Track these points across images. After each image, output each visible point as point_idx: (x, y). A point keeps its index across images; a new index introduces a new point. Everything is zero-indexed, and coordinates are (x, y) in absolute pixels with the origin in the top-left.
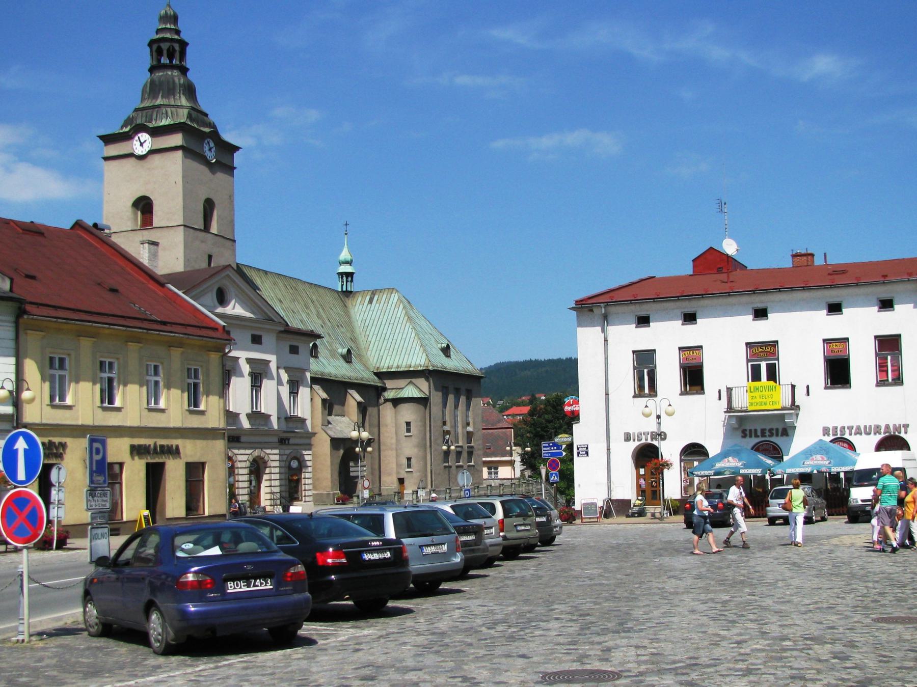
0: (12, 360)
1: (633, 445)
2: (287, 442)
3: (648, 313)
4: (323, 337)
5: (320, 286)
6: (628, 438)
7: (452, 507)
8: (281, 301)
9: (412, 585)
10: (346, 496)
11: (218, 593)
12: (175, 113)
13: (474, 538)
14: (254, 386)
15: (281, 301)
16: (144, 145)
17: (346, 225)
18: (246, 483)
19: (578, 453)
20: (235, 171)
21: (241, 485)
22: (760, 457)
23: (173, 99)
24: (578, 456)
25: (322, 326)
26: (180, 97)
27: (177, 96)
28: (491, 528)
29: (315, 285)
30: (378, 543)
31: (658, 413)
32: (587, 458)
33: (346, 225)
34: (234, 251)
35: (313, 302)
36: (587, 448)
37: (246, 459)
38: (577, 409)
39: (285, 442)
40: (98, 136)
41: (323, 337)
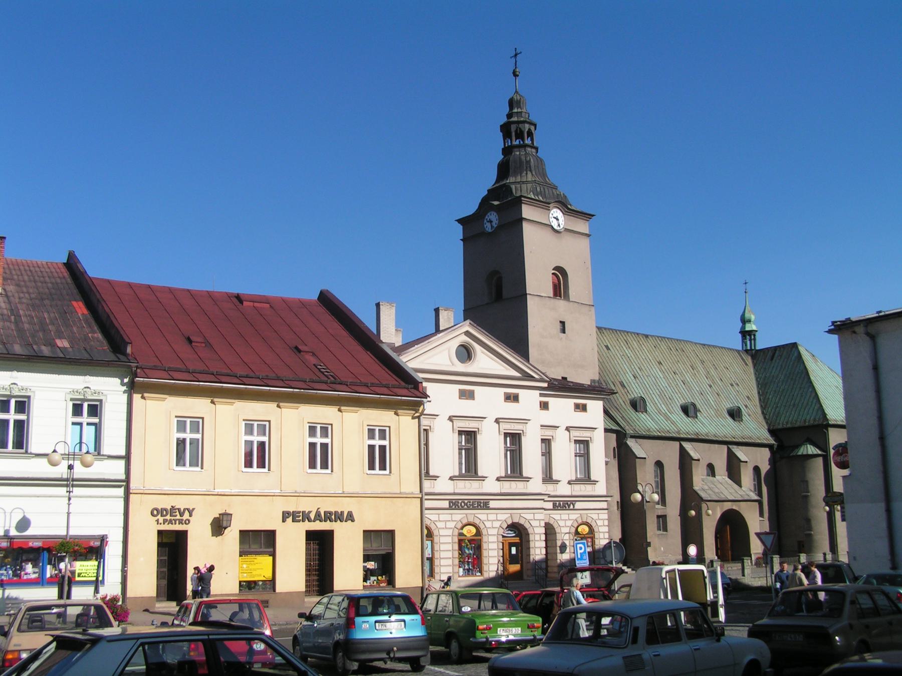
0: (830, 429)
2: (572, 507)
5: (713, 346)
8: (660, 363)
9: (225, 672)
10: (366, 569)
12: (519, 189)
15: (660, 363)
17: (746, 283)
20: (462, 238)
21: (443, 555)
23: (519, 177)
25: (710, 386)
26: (527, 174)
27: (524, 174)
28: (7, 615)
29: (709, 346)
33: (746, 283)
35: (702, 362)
39: (569, 506)
40: (456, 220)
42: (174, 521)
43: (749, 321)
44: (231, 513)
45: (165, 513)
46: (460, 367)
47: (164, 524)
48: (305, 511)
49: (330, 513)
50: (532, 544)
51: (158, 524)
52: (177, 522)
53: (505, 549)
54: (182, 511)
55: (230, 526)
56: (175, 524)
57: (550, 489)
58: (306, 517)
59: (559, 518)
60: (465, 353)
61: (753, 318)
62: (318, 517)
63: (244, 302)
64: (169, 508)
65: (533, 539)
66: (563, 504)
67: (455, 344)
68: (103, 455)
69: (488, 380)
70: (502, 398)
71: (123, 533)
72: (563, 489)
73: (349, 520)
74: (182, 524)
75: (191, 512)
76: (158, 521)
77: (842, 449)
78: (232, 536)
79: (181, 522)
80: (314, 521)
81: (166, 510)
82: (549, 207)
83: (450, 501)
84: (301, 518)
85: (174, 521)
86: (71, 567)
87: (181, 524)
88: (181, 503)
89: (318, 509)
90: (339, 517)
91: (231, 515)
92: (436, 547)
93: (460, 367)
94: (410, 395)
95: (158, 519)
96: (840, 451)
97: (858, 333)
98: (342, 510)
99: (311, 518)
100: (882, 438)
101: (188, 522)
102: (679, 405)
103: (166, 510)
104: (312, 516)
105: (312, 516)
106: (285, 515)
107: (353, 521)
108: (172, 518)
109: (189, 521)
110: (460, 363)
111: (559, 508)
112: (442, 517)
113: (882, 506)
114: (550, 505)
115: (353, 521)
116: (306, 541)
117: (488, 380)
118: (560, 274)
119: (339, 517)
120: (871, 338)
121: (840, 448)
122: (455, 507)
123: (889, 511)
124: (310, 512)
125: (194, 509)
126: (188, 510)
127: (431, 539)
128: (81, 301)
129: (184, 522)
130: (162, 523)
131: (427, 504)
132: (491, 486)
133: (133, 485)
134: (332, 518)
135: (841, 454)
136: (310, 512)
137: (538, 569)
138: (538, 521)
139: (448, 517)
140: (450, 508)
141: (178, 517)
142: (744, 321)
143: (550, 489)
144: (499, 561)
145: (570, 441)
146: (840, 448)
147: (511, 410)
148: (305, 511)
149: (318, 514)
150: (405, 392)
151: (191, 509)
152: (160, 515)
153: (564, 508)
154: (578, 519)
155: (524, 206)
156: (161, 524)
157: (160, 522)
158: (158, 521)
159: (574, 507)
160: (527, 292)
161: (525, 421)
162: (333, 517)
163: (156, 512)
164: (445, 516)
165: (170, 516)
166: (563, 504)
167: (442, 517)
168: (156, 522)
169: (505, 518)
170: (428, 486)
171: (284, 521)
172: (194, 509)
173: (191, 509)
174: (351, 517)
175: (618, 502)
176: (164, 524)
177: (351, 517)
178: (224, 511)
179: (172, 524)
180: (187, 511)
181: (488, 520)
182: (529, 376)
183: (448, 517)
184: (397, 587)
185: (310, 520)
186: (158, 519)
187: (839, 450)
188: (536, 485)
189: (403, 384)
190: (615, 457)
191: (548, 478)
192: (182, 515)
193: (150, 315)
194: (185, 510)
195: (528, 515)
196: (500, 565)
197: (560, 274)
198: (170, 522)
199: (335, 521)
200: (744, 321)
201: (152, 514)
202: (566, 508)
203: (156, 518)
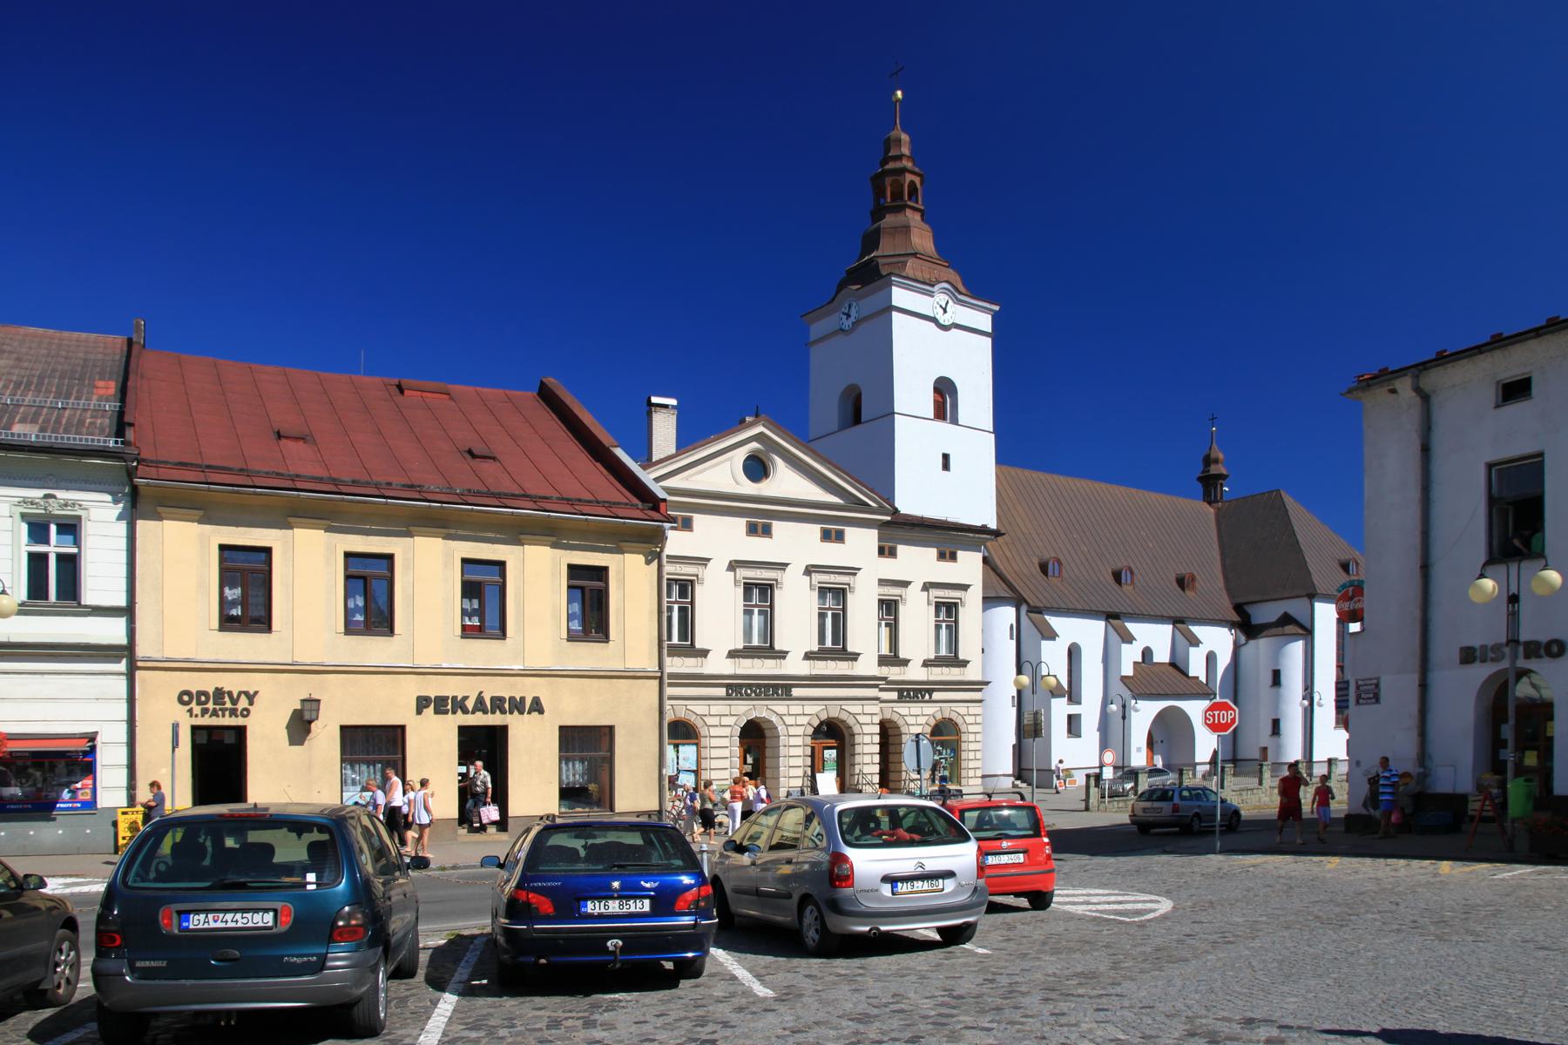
1: (1480, 673)
2: (927, 697)
3: (1527, 370)
4: (1004, 534)
6: (1468, 656)
7: (585, 847)
11: (288, 963)
13: (164, 965)
14: (883, 619)
16: (948, 309)
18: (894, 751)
19: (1358, 698)
22: (151, 841)
24: (1358, 703)
30: (1156, 830)
31: (1514, 590)
32: (1376, 706)
34: (850, 427)
36: (1377, 686)
37: (805, 723)
38: (1358, 606)
39: (923, 697)
41: (1004, 534)
42: (220, 713)
43: (1216, 461)
44: (317, 698)
45: (203, 698)
46: (749, 488)
47: (203, 716)
48: (456, 697)
49: (501, 699)
50: (858, 749)
51: (191, 716)
52: (227, 713)
53: (821, 760)
54: (235, 696)
55: (317, 719)
56: (223, 716)
57: (894, 673)
58: (459, 705)
59: (907, 713)
60: (757, 468)
61: (1221, 456)
62: (480, 705)
63: (406, 392)
64: (211, 691)
65: (861, 742)
66: (913, 693)
67: (741, 455)
68: (86, 606)
69: (795, 511)
70: (818, 535)
71: (128, 733)
72: (915, 673)
73: (535, 711)
74: (237, 716)
75: (251, 698)
76: (190, 711)
77: (1353, 590)
78: (326, 737)
79: (233, 712)
80: (473, 713)
81: (205, 694)
82: (933, 292)
83: (728, 686)
84: (449, 707)
85: (220, 713)
86: (843, 787)
87: (233, 716)
88: (232, 683)
89: (481, 692)
90: (517, 706)
91: (319, 701)
92: (704, 753)
93: (749, 488)
94: (641, 517)
95: (192, 709)
96: (1350, 594)
97: (1337, 561)
98: (523, 695)
99: (466, 708)
100: (1425, 568)
101: (246, 713)
102: (1110, 571)
103: (185, 694)
104: (470, 704)
105: (470, 704)
106: (422, 703)
107: (541, 711)
108: (218, 707)
109: (248, 710)
110: (750, 482)
111: (908, 699)
112: (714, 710)
113: (1414, 678)
114: (894, 695)
115: (541, 711)
116: (560, 750)
117: (795, 511)
118: (945, 392)
119: (517, 706)
120: (1422, 398)
121: (1351, 589)
122: (736, 695)
123: (1424, 686)
124: (465, 698)
125: (256, 693)
126: (246, 693)
127: (696, 741)
128: (116, 382)
129: (239, 713)
130: (200, 715)
131: (669, 691)
132: (795, 665)
133: (142, 650)
134: (505, 708)
135: (1351, 599)
136: (465, 698)
137: (865, 784)
138: (870, 716)
139: (725, 710)
140: (728, 697)
141: (229, 705)
142: (1208, 461)
143: (894, 673)
144: (805, 772)
145: (928, 604)
146: (1351, 589)
147: (831, 554)
148: (456, 697)
149: (480, 701)
150: (638, 514)
151: (252, 693)
152: (194, 701)
153: (916, 699)
154: (935, 715)
155: (894, 289)
156: (196, 716)
157: (195, 712)
158: (190, 711)
159: (930, 697)
160: (896, 411)
161: (852, 571)
162: (507, 706)
163: (185, 698)
164: (718, 708)
165: (214, 704)
166: (913, 693)
167: (714, 710)
168: (188, 714)
169: (816, 712)
170: (675, 665)
171: (419, 712)
172: (256, 693)
173: (252, 693)
174: (537, 707)
175: (1013, 697)
176: (203, 716)
177: (537, 707)
178: (308, 696)
179: (218, 716)
180: (243, 696)
181: (789, 715)
182: (858, 502)
183: (725, 710)
184: (617, 811)
185: (465, 711)
186: (192, 709)
187: (1347, 593)
188: (867, 666)
189: (636, 501)
190: (1012, 638)
191: (892, 658)
192: (235, 702)
193: (399, 463)
194: (240, 693)
195: (855, 708)
196: (806, 779)
197: (945, 392)
198: (215, 713)
199: (511, 713)
200: (1208, 461)
201: (181, 701)
202: (918, 698)
203: (188, 707)
